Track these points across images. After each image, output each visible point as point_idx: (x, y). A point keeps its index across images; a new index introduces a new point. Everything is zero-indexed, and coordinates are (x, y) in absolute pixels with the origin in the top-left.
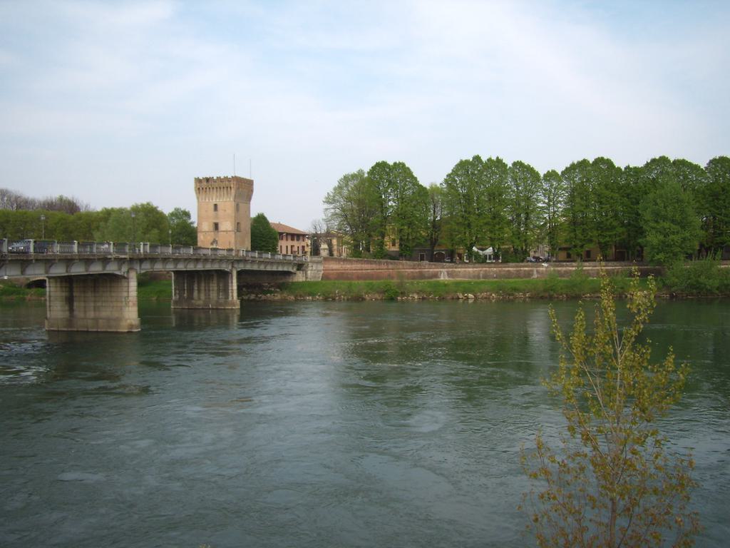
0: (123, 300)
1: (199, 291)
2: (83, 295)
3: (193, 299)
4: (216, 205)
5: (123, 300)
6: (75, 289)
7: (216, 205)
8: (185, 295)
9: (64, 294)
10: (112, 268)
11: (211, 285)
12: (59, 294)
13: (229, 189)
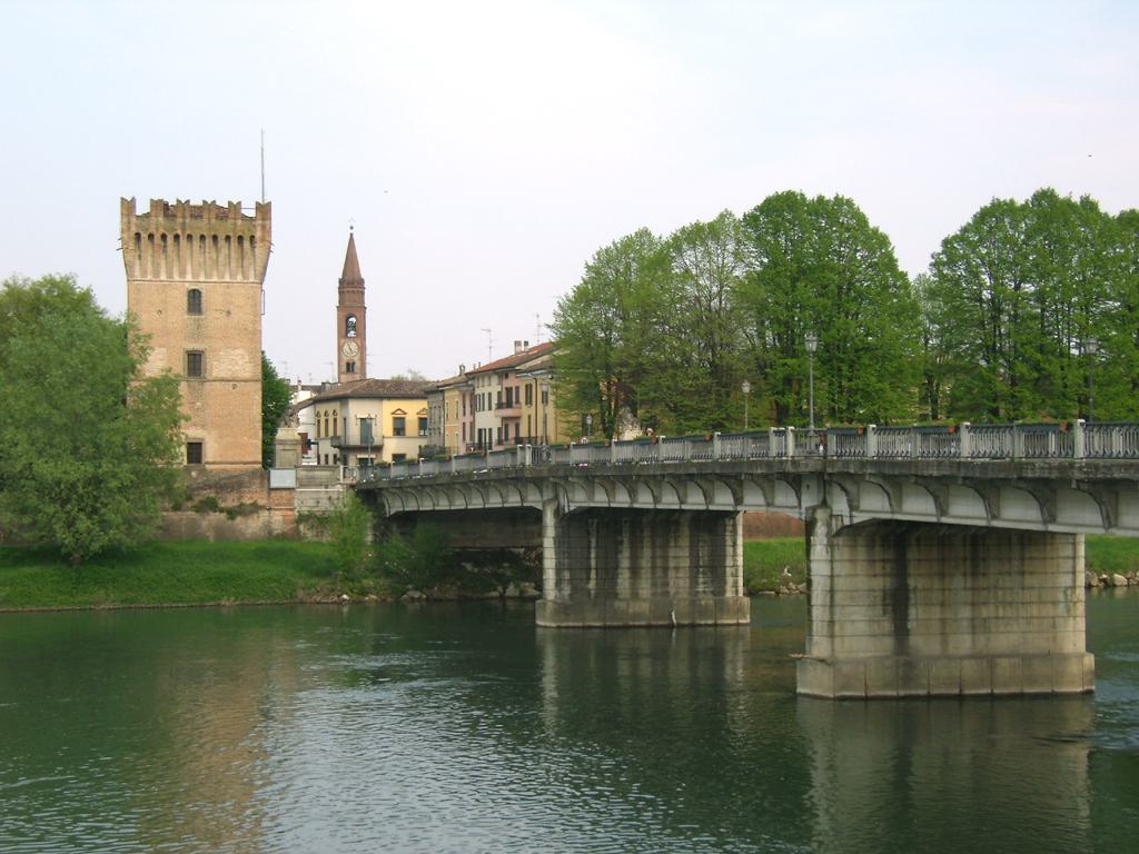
0: (1061, 597)
1: (635, 571)
2: (937, 584)
3: (616, 596)
4: (195, 298)
5: (1061, 597)
6: (911, 570)
7: (195, 298)
8: (592, 585)
9: (879, 583)
10: (1019, 514)
11: (672, 553)
12: (862, 582)
13: (247, 244)
